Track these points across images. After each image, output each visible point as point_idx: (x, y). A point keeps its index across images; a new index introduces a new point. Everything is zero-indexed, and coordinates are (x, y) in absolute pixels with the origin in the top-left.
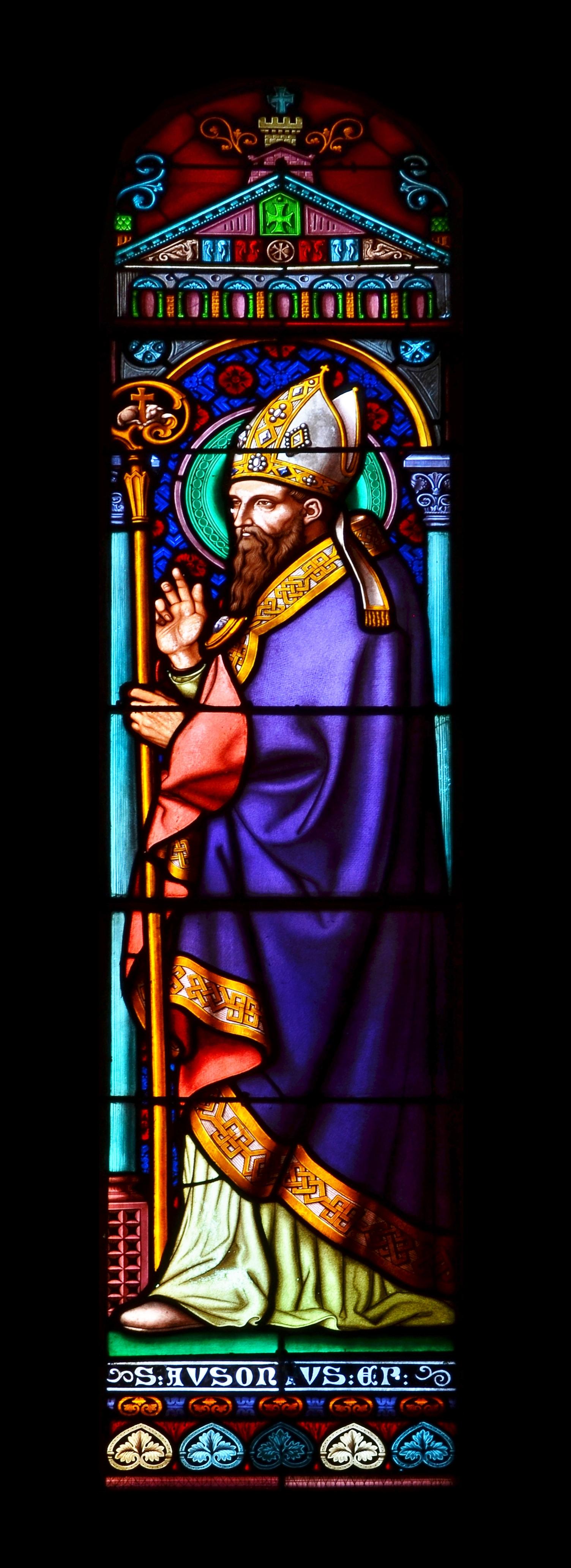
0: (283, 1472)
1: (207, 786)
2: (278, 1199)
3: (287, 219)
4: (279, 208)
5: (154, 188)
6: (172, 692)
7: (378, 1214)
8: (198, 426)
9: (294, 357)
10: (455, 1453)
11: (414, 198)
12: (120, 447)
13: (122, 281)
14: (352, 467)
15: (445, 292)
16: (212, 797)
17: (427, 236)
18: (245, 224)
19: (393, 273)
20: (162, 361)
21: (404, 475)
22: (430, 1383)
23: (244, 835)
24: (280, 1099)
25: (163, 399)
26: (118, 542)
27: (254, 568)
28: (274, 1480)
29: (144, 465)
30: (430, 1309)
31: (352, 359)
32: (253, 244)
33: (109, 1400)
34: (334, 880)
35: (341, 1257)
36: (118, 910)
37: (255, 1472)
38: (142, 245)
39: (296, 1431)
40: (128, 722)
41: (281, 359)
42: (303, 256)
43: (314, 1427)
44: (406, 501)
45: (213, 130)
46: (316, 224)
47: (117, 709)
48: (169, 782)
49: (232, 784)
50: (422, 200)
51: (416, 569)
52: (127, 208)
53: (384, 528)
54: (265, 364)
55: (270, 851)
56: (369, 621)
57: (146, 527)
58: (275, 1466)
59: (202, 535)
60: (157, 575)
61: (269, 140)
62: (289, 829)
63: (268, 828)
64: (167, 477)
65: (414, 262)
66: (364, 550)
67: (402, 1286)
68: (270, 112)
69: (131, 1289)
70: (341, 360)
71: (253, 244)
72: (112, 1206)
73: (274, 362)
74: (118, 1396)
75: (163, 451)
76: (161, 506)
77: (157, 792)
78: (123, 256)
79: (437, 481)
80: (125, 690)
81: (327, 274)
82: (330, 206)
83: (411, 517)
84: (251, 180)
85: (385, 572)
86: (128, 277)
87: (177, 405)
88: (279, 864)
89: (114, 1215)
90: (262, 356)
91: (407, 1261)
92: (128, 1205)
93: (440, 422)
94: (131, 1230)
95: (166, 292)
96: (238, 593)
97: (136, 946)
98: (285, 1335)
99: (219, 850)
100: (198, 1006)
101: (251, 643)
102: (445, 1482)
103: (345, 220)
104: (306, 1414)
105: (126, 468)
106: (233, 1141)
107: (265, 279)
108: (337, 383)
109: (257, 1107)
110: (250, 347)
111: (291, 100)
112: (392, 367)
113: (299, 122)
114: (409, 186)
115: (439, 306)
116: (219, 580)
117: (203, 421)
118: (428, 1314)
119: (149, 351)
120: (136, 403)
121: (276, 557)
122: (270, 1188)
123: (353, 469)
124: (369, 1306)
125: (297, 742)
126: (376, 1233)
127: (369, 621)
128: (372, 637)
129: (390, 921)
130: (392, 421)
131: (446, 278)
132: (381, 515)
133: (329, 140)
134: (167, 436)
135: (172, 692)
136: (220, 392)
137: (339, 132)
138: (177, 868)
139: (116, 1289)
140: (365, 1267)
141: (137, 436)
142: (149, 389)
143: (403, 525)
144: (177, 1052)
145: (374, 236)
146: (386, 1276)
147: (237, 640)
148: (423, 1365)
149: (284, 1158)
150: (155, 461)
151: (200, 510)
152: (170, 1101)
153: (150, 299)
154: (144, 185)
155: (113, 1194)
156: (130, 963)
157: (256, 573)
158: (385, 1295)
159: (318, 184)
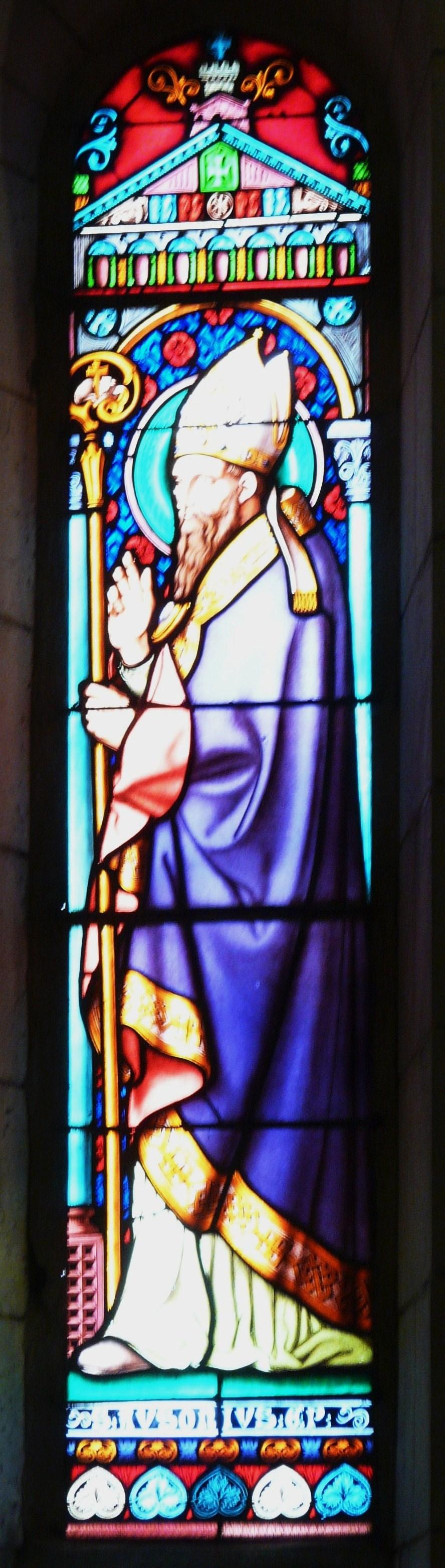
0: (221, 1519)
1: (155, 789)
2: (216, 1230)
3: (226, 172)
4: (219, 159)
5: (107, 144)
6: (123, 688)
7: (305, 1246)
8: (146, 401)
9: (230, 323)
10: (372, 1499)
11: (339, 142)
12: (76, 427)
13: (80, 246)
14: (282, 438)
15: (365, 243)
16: (159, 799)
17: (350, 184)
18: (186, 179)
19: (319, 224)
20: (115, 331)
21: (329, 445)
22: (350, 1424)
23: (186, 842)
24: (219, 1125)
25: (116, 373)
26: (76, 525)
27: (195, 553)
28: (212, 1529)
29: (99, 442)
30: (351, 1346)
31: (281, 323)
32: (196, 200)
33: (70, 1443)
34: (265, 887)
35: (273, 1291)
36: (77, 924)
37: (196, 1520)
38: (98, 206)
39: (232, 1476)
40: (85, 723)
41: (218, 325)
42: (240, 210)
43: (249, 1472)
44: (330, 474)
45: (160, 80)
46: (252, 176)
47: (75, 709)
48: (121, 784)
49: (175, 787)
50: (345, 145)
51: (340, 546)
52: (83, 168)
53: (310, 505)
54: (205, 332)
55: (210, 856)
56: (299, 605)
57: (102, 510)
58: (214, 1513)
59: (150, 516)
60: (110, 562)
61: (209, 89)
62: (224, 836)
63: (209, 832)
64: (119, 456)
65: (339, 212)
66: (292, 528)
67: (326, 1322)
68: (210, 59)
69: (89, 1328)
70: (272, 324)
71: (196, 200)
72: (71, 1241)
73: (213, 329)
74: (77, 1441)
75: (117, 429)
76: (114, 487)
77: (110, 797)
78: (81, 220)
79: (360, 449)
80: (83, 687)
81: (261, 229)
82: (262, 156)
83: (336, 491)
84: (192, 133)
85: (313, 549)
86: (85, 242)
87: (127, 381)
88: (219, 871)
89: (74, 1250)
90: (203, 322)
91: (331, 1296)
92: (86, 1240)
93: (362, 386)
94: (88, 1265)
95: (119, 257)
96: (182, 580)
97: (91, 966)
98: (222, 1376)
99: (165, 858)
100: (145, 1026)
101: (193, 630)
102: (363, 1529)
103: (276, 170)
104: (242, 1459)
105: (83, 447)
106: (177, 1170)
107: (207, 236)
108: (270, 348)
109: (200, 1134)
110: (193, 314)
111: (229, 44)
112: (319, 328)
113: (235, 68)
114: (334, 129)
115: (360, 260)
116: (164, 566)
117: (151, 394)
118: (348, 1352)
119: (103, 321)
120: (92, 377)
121: (215, 539)
122: (210, 1220)
123: (283, 441)
124: (296, 1346)
125: (235, 738)
126: (304, 1266)
127: (299, 605)
128: (301, 622)
129: (317, 930)
130: (317, 388)
131: (366, 229)
132: (308, 492)
133: (263, 85)
134: (118, 414)
135: (123, 688)
136: (165, 363)
137: (271, 77)
138: (128, 877)
139: (75, 1328)
140: (290, 1369)
141: (93, 413)
142: (103, 363)
143: (329, 500)
144: (128, 1075)
145: (301, 185)
146: (311, 1311)
147: (180, 630)
148: (345, 1406)
149: (222, 1188)
150: (109, 440)
151: (149, 491)
152: (122, 1128)
153: (104, 265)
154: (98, 144)
155: (73, 1228)
156: (87, 981)
157: (199, 556)
158: (310, 1333)
159: (253, 132)
